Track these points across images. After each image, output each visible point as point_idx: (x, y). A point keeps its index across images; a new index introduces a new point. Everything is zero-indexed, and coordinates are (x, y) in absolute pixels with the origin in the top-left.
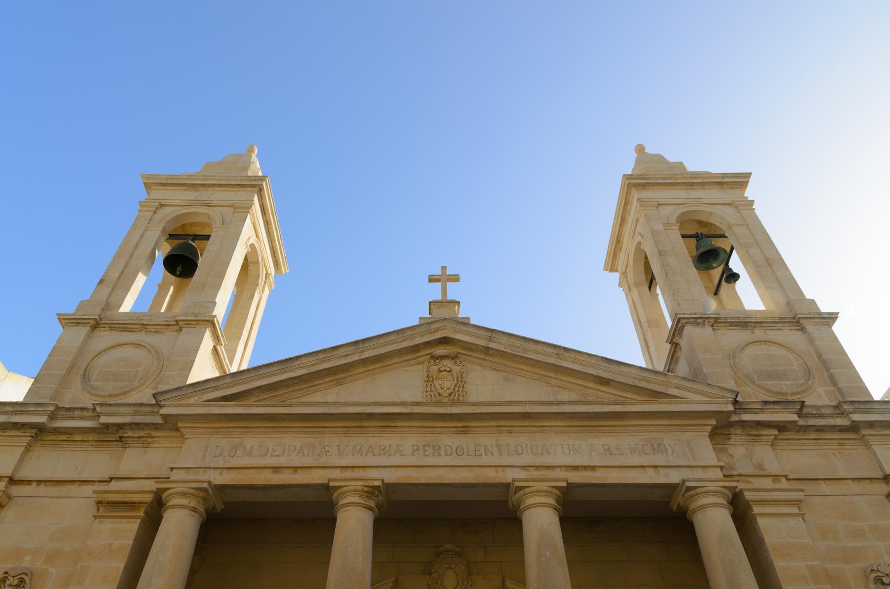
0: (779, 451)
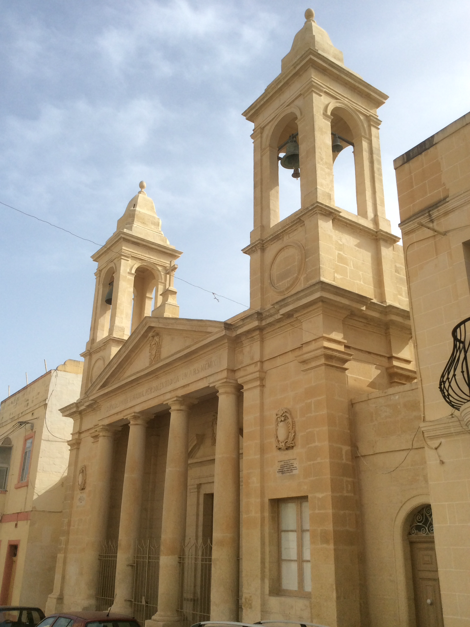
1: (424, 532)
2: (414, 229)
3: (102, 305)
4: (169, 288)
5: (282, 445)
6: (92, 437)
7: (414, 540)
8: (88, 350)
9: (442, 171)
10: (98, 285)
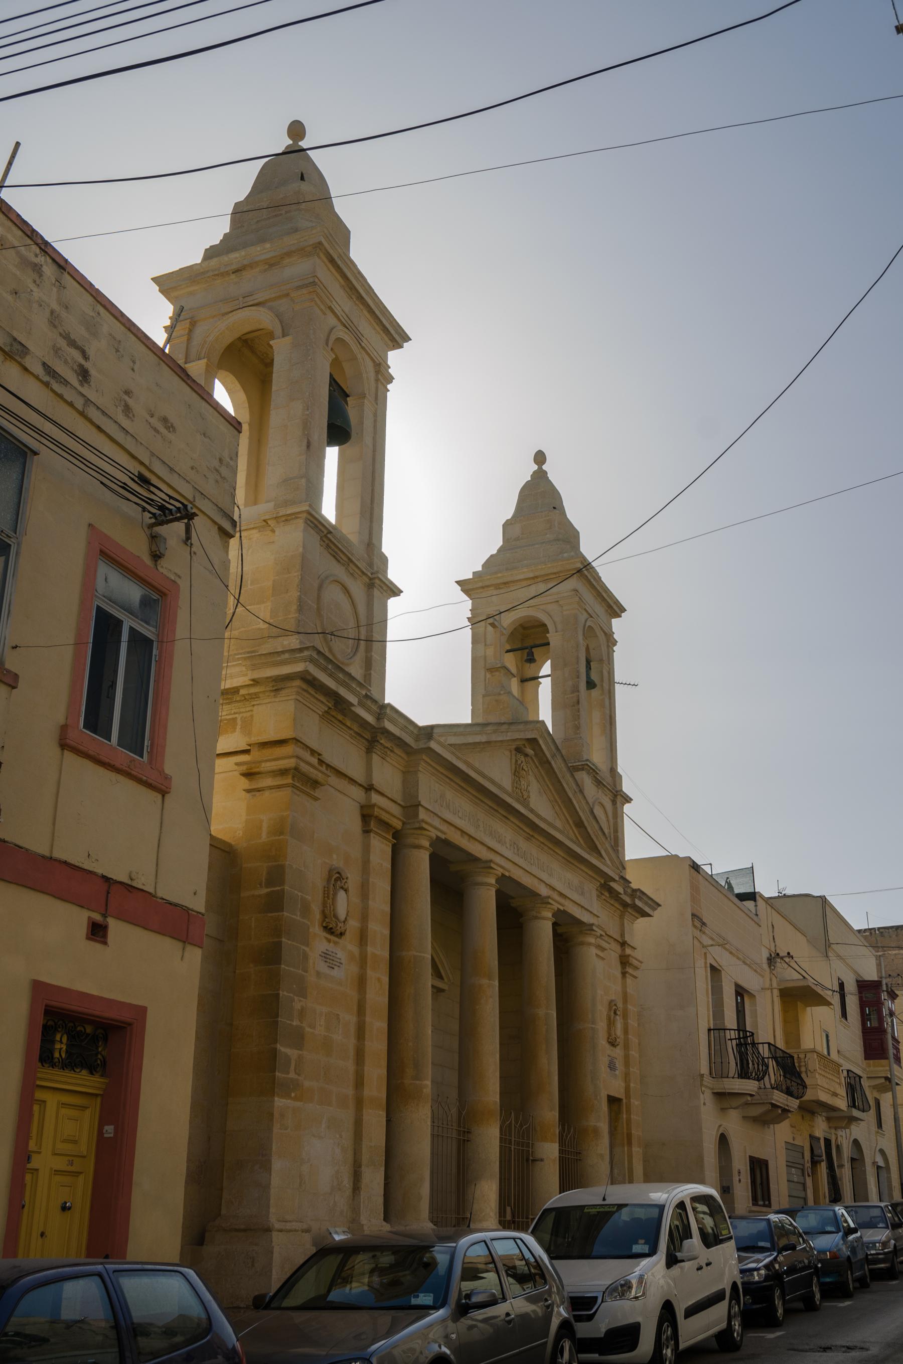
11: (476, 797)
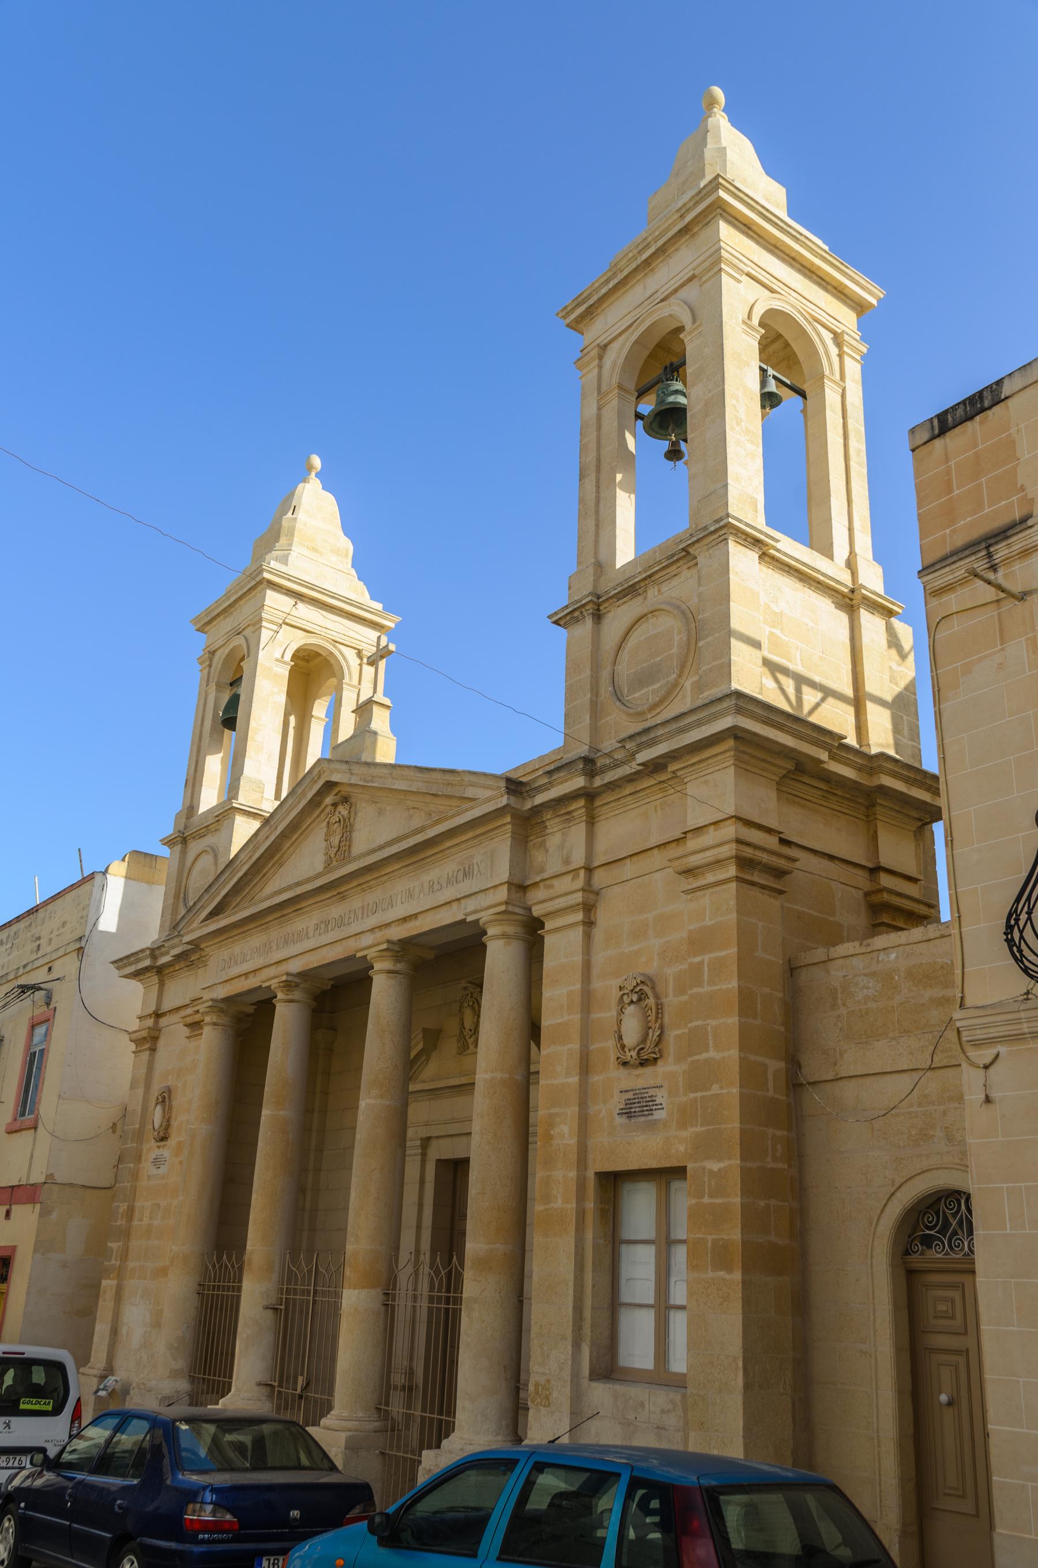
0: (603, 822)
1: (939, 1249)
2: (952, 584)
3: (213, 728)
4: (373, 696)
5: (631, 1055)
6: (185, 1025)
7: (918, 1266)
8: (179, 831)
9: (1019, 459)
10: (205, 685)
11: (257, 927)
